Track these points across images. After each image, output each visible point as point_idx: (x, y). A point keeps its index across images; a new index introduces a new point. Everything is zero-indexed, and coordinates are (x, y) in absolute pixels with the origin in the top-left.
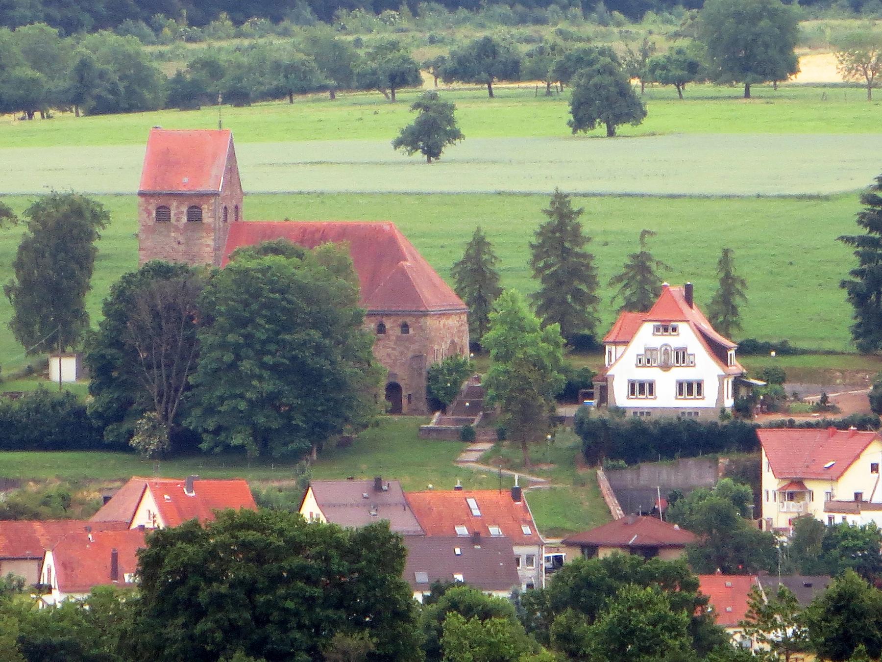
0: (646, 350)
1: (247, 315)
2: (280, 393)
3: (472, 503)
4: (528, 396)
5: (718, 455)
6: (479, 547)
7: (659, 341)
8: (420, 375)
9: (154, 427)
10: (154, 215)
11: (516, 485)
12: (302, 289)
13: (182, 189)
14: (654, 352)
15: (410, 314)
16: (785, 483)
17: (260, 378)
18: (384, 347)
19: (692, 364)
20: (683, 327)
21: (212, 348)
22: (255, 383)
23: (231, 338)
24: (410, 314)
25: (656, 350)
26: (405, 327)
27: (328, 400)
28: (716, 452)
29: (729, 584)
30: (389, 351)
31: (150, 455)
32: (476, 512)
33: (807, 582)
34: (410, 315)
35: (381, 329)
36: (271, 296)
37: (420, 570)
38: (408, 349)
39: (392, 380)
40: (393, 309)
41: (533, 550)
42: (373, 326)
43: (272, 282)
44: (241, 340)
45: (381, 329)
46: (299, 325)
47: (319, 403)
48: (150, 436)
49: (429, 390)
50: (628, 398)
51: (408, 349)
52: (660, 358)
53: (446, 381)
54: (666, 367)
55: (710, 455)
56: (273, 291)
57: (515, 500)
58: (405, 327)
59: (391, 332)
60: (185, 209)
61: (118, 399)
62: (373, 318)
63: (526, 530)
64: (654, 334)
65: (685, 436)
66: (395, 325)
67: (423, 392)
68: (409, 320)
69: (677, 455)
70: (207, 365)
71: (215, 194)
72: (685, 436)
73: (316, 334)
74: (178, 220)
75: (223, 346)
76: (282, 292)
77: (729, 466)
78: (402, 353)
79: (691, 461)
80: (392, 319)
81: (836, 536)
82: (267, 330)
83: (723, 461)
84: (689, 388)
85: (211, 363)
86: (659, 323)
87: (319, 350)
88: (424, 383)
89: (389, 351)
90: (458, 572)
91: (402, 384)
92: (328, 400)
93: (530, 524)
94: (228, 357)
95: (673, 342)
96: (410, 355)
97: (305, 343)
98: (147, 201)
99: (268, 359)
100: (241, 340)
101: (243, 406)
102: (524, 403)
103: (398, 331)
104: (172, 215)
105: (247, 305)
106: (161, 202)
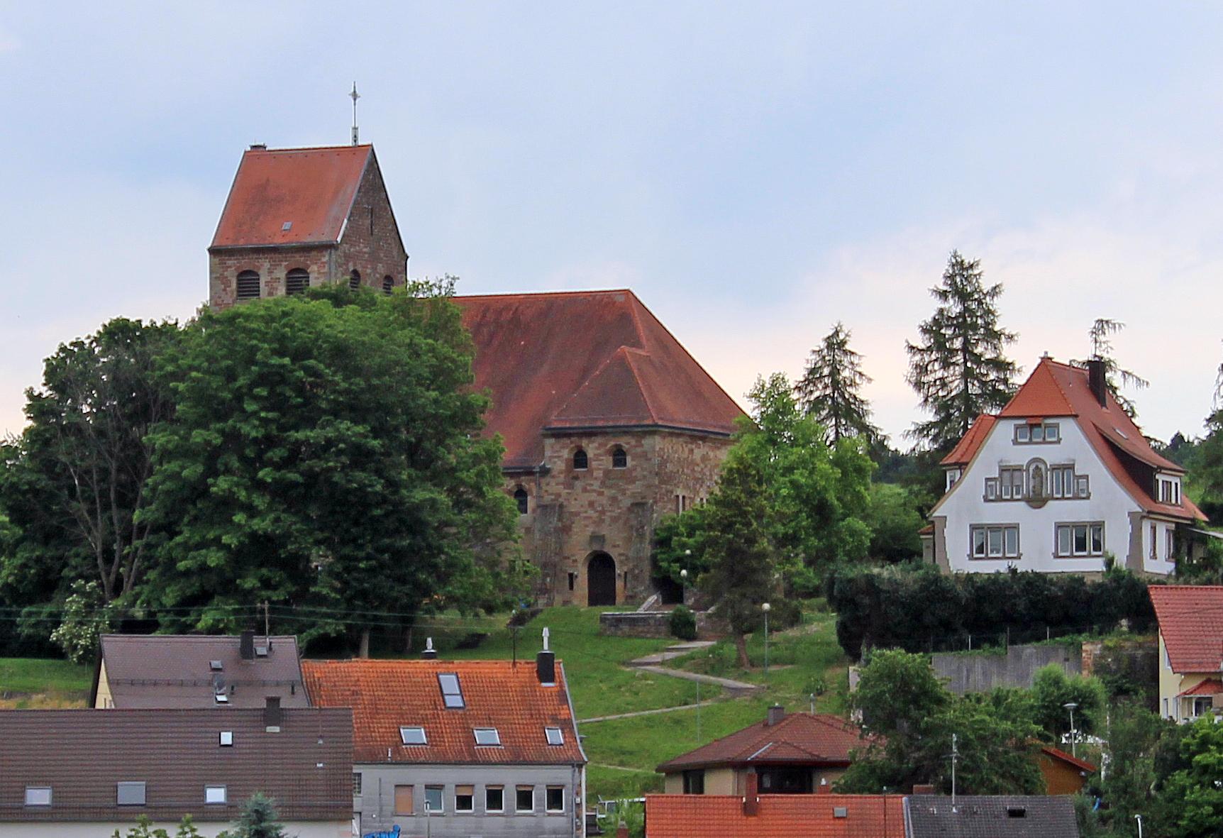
0: (1003, 470)
1: (227, 395)
2: (287, 536)
3: (449, 683)
4: (737, 535)
5: (1082, 638)
6: (277, 729)
7: (1022, 455)
8: (641, 536)
9: (89, 606)
10: (234, 285)
11: (546, 648)
12: (340, 353)
13: (278, 241)
14: (1017, 474)
15: (625, 431)
16: (1194, 683)
17: (251, 511)
18: (585, 490)
19: (1081, 495)
20: (1069, 429)
21: (167, 455)
22: (239, 518)
23: (198, 436)
24: (625, 431)
25: (1018, 469)
26: (619, 456)
27: (382, 551)
28: (1080, 632)
29: (840, 811)
30: (593, 496)
31: (79, 658)
32: (454, 701)
33: (1016, 807)
34: (626, 433)
35: (580, 459)
36: (275, 361)
37: (204, 795)
38: (624, 492)
39: (596, 547)
40: (600, 424)
41: (561, 775)
42: (566, 454)
43: (282, 338)
44: (217, 440)
45: (580, 459)
46: (325, 412)
47: (362, 554)
48: (81, 623)
49: (654, 561)
50: (971, 557)
51: (624, 492)
52: (1027, 483)
53: (684, 546)
54: (1037, 500)
55: (1066, 639)
56: (281, 354)
57: (542, 681)
58: (619, 456)
59: (594, 464)
60: (281, 274)
61: (39, 560)
62: (567, 441)
63: (555, 736)
64: (1015, 442)
65: (1022, 605)
66: (601, 451)
67: (647, 567)
68: (626, 442)
69: (1003, 638)
70: (156, 484)
71: (331, 246)
72: (1022, 605)
73: (349, 429)
74: (270, 294)
75: (185, 453)
76: (300, 355)
77: (1102, 657)
78: (614, 499)
79: (1029, 649)
80: (599, 440)
81: (1187, 745)
82: (265, 422)
83: (1091, 649)
84: (1084, 538)
85: (163, 482)
86: (1023, 422)
87: (360, 456)
88: (648, 550)
89: (593, 496)
90: (215, 783)
91: (614, 553)
92: (382, 551)
93: (566, 725)
94: (192, 471)
95: (1051, 454)
96: (626, 502)
97: (330, 443)
98: (222, 263)
99: (265, 474)
100: (217, 440)
101: (214, 558)
102: (733, 552)
103: (608, 462)
104: (262, 285)
105: (231, 376)
106: (245, 263)
